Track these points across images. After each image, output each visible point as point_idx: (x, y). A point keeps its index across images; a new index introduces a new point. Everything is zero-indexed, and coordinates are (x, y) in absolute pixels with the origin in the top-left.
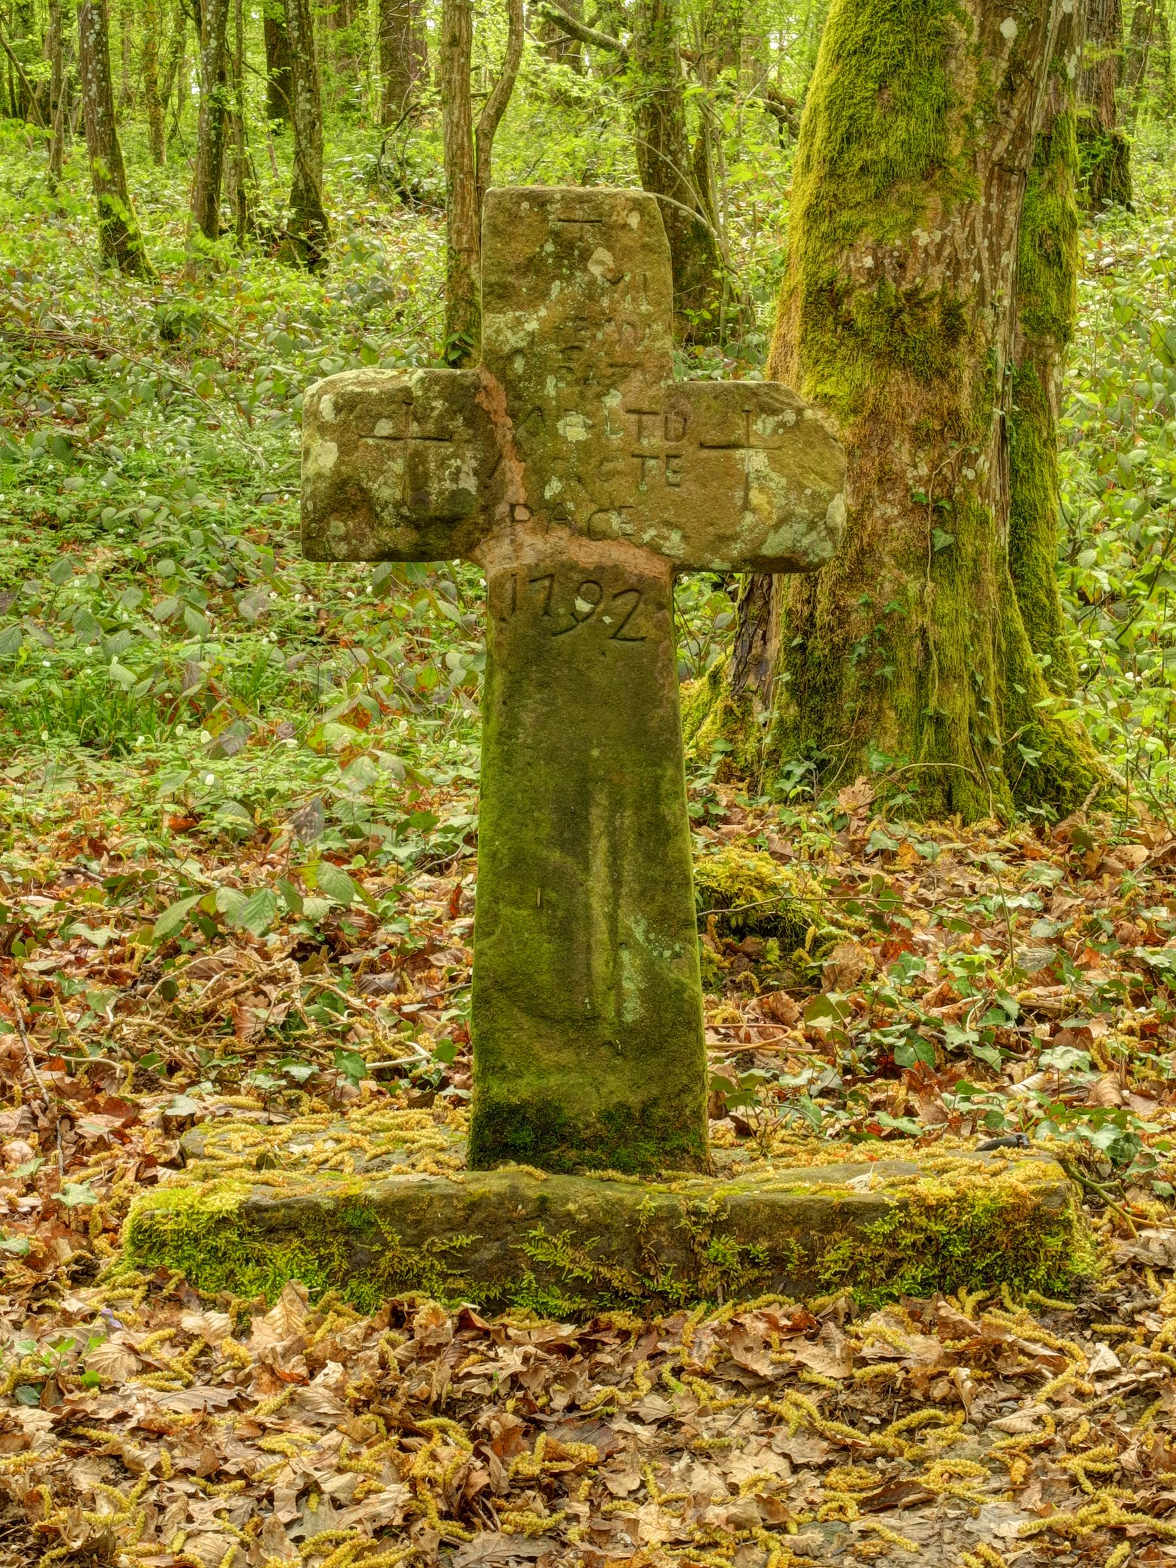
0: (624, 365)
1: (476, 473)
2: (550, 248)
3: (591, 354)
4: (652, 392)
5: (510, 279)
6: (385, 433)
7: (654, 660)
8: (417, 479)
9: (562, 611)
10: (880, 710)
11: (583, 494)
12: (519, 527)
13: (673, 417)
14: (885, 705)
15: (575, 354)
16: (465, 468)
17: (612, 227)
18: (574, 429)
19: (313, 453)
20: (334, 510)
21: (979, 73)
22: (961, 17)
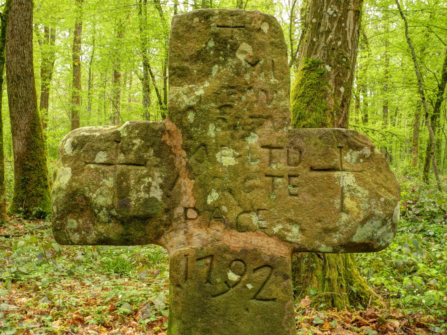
0: (260, 117)
1: (162, 187)
2: (211, 44)
3: (238, 110)
4: (278, 134)
5: (186, 64)
6: (102, 161)
7: (282, 315)
8: (122, 190)
9: (218, 280)
10: (312, 276)
11: (233, 201)
12: (190, 223)
13: (292, 150)
14: (313, 275)
15: (228, 110)
16: (154, 184)
17: (252, 30)
18: (227, 158)
19: (58, 175)
20: (70, 212)
21: (335, 101)
22: (329, 86)
